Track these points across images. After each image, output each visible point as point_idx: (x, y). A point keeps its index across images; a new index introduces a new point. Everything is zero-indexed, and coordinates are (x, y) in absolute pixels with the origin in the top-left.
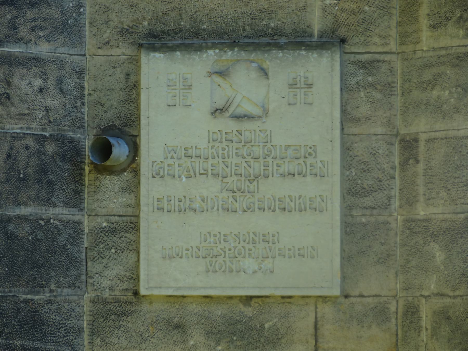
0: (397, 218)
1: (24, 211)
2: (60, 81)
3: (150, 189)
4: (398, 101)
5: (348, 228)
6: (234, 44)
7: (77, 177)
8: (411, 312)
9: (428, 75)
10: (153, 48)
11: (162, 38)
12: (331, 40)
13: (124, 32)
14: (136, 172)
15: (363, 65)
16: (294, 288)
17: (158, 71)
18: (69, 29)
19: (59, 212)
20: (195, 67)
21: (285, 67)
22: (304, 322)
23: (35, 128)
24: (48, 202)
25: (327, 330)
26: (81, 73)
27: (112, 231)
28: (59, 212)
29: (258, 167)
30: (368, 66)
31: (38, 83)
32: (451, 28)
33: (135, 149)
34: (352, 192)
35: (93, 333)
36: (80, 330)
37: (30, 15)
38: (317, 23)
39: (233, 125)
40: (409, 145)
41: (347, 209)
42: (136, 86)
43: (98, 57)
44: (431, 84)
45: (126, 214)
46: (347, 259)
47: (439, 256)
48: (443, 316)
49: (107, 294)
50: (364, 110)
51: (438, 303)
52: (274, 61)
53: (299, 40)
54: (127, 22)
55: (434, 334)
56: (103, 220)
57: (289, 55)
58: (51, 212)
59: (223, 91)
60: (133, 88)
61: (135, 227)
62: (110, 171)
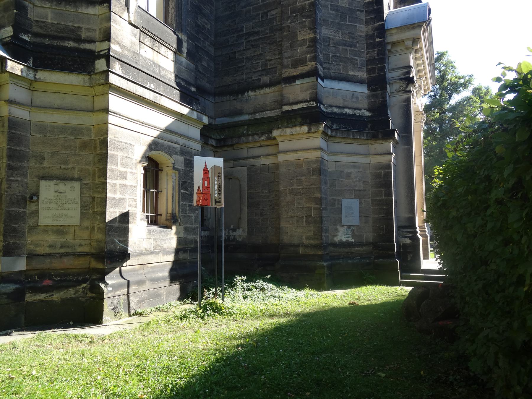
0: (91, 211)
1: (13, 209)
2: (22, 185)
3: (41, 205)
4: (91, 191)
5: (82, 213)
6: (59, 180)
7: (26, 203)
8: (93, 228)
9: (97, 186)
10: (42, 179)
11: (45, 178)
12: (79, 179)
13: (36, 176)
14: (38, 202)
15: (85, 184)
16: (269, 155)
17: (43, 184)
18: (25, 175)
19: (21, 210)
20: (52, 183)
21: (69, 184)
22: (72, 230)
23: (16, 193)
24: (19, 208)
25: (77, 231)
26: (27, 184)
27: (33, 213)
28: (21, 210)
29: (64, 202)
30: (86, 184)
31: (17, 185)
32: (102, 178)
33: (38, 198)
34: (82, 207)
35: (28, 232)
36: (25, 232)
37: (16, 172)
38: (76, 176)
39: (59, 194)
40: (93, 198)
41: (81, 210)
42: (39, 186)
43: (31, 181)
44: (98, 188)
45: (396, 67)
46: (81, 218)
47: (99, 218)
48: (99, 228)
49: (31, 225)
50: (85, 192)
51: (99, 226)
52: (67, 183)
53: (73, 179)
54: (37, 174)
55: (97, 231)
56: (5, 75)
57: (71, 182)
58: (20, 209)
59: (57, 188)
60: (38, 187)
61: (38, 212)
62: (33, 202)
